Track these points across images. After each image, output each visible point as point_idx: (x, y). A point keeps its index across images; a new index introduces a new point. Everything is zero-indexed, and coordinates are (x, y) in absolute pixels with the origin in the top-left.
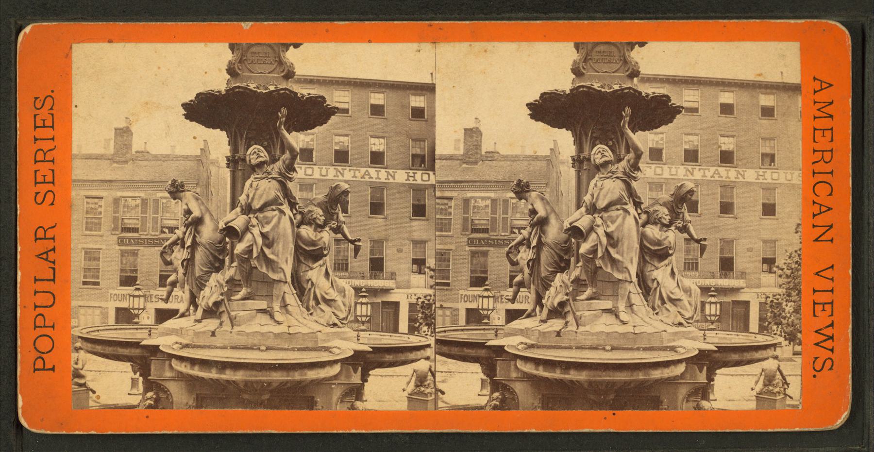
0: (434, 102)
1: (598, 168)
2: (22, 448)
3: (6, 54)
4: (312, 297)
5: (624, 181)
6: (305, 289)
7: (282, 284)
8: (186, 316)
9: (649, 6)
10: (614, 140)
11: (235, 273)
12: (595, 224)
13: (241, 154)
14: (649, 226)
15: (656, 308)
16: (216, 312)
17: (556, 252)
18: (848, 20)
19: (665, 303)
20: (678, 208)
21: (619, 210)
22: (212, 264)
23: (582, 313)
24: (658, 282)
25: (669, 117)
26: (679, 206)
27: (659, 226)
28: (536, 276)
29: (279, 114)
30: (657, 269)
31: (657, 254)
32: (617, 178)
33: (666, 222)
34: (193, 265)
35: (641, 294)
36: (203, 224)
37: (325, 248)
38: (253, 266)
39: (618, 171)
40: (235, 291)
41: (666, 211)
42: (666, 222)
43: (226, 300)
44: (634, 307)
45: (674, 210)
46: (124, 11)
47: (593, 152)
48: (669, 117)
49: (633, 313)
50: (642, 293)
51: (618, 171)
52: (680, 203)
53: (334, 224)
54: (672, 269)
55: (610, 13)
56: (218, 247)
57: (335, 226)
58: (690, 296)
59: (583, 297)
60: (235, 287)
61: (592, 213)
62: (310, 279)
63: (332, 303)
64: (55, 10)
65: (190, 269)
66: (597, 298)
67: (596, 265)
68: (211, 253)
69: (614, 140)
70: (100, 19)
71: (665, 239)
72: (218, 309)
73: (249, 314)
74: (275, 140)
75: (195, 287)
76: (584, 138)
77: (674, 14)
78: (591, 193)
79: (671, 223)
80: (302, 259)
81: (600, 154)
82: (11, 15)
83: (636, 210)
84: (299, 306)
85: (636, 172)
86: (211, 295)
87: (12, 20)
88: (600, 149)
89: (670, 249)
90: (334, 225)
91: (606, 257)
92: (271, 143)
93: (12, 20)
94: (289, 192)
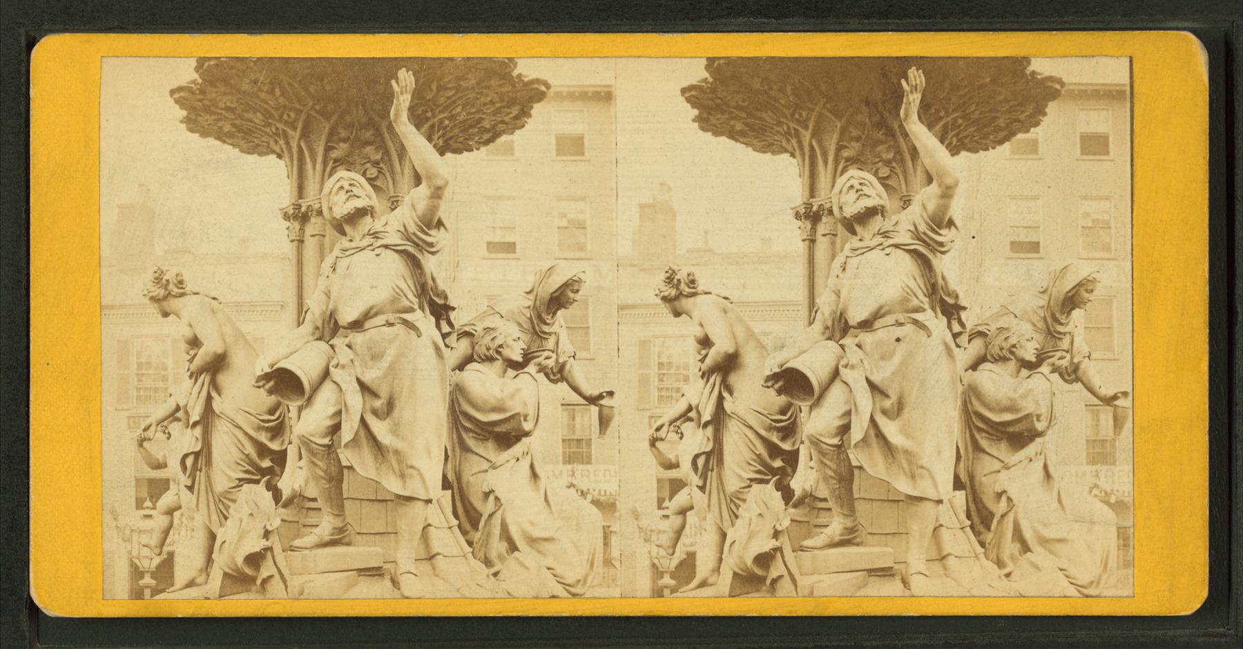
3: (13, 78)
4: (1009, 534)
5: (915, 253)
6: (992, 515)
7: (420, 504)
10: (381, 165)
11: (307, 482)
13: (310, 200)
14: (987, 366)
15: (496, 561)
16: (764, 579)
17: (246, 434)
18: (1206, 26)
19: (1029, 550)
21: (901, 324)
23: (816, 578)
24: (1009, 499)
25: (515, 111)
26: (548, 318)
28: (203, 492)
30: (494, 467)
31: (490, 432)
33: (1030, 356)
34: (209, 462)
35: (456, 530)
36: (228, 368)
37: (1038, 417)
41: (515, 331)
42: (1030, 356)
43: (278, 550)
44: (951, 561)
45: (533, 328)
47: (326, 190)
48: (1030, 109)
49: (948, 576)
50: (972, 527)
51: (388, 229)
52: (1063, 313)
54: (532, 467)
55: (868, 19)
56: (269, 421)
57: (1065, 363)
58: (578, 527)
59: (309, 539)
60: (306, 517)
63: (1059, 546)
65: (201, 477)
66: (346, 540)
67: (339, 461)
68: (251, 438)
69: (381, 165)
70: (146, 28)
71: (513, 396)
73: (347, 577)
74: (910, 164)
76: (309, 166)
77: (959, 19)
79: (528, 357)
84: (977, 557)
86: (241, 538)
87: (22, 31)
88: (852, 182)
89: (525, 420)
91: (364, 441)
92: (898, 170)
93: (22, 31)
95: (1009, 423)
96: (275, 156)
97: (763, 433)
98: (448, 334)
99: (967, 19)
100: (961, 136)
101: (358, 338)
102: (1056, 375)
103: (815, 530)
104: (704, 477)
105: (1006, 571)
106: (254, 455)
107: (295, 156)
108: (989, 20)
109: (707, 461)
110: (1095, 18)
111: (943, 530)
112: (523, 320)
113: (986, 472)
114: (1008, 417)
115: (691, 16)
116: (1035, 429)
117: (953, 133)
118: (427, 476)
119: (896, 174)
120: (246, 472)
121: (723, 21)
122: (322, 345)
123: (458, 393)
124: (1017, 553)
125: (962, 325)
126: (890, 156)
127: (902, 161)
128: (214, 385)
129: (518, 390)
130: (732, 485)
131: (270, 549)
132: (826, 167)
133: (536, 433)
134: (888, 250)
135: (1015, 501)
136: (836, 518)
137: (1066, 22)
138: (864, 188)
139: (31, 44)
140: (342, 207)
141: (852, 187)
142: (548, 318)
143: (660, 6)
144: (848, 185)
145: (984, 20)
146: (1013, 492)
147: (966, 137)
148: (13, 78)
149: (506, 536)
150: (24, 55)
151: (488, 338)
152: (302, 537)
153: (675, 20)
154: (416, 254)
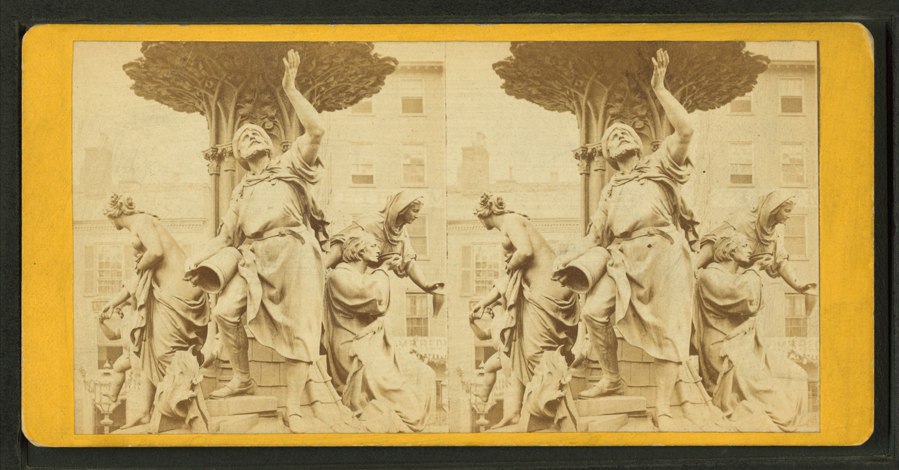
0: (291, 42)
1: (616, 162)
2: (27, 460)
3: (9, 57)
5: (661, 183)
6: (718, 373)
7: (304, 365)
8: (143, 424)
9: (668, 5)
11: (222, 349)
12: (610, 262)
13: (224, 145)
14: (714, 265)
15: (359, 406)
17: (178, 314)
18: (872, 19)
20: (768, 235)
21: (652, 235)
22: (182, 335)
23: (590, 418)
24: (730, 362)
26: (396, 231)
27: (361, 264)
28: (147, 357)
29: (653, 60)
30: (357, 338)
31: (355, 313)
32: (648, 178)
33: (745, 258)
34: (521, 334)
36: (165, 266)
37: (751, 302)
38: (249, 336)
39: (280, 165)
40: (590, 381)
41: (372, 240)
42: (745, 258)
43: (201, 398)
44: (688, 407)
45: (386, 237)
46: (130, 13)
47: (236, 138)
49: (685, 417)
50: (703, 382)
51: (280, 165)
53: (396, 259)
55: (628, 13)
56: (194, 305)
58: (418, 382)
60: (222, 374)
61: (606, 242)
62: (356, 356)
63: (766, 395)
64: (60, 12)
66: (250, 391)
67: (245, 334)
68: (181, 317)
70: (106, 21)
71: (371, 287)
72: (186, 411)
73: (251, 418)
75: (155, 374)
78: (234, 209)
80: (340, 320)
81: (248, 140)
82: (15, 17)
83: (317, 236)
84: (706, 403)
85: (313, 168)
88: (616, 132)
90: (768, 262)
91: (263, 319)
92: (650, 123)
93: (16, 22)
94: (311, 204)
95: (730, 307)
96: (199, 113)
97: (552, 313)
98: (324, 242)
99: (699, 14)
100: (695, 98)
101: (259, 245)
102: (764, 272)
103: (589, 384)
104: (509, 345)
105: (728, 413)
106: (184, 330)
107: (214, 113)
108: (715, 15)
109: (511, 334)
110: (792, 13)
111: (682, 384)
112: (378, 232)
113: (713, 341)
114: (729, 302)
115: (500, 11)
116: (749, 311)
117: (689, 96)
118: (309, 345)
119: (648, 126)
120: (549, 342)
121: (523, 15)
122: (233, 250)
123: (331, 285)
124: (735, 401)
125: (326, 235)
126: (644, 113)
127: (652, 117)
128: (155, 278)
129: (375, 283)
130: (530, 351)
131: (195, 398)
132: (597, 121)
133: (388, 314)
134: (642, 181)
135: (734, 363)
136: (605, 375)
137: (771, 16)
138: (256, 137)
139: (22, 32)
140: (248, 150)
141: (616, 135)
142: (396, 231)
143: (477, 4)
144: (613, 134)
145: (712, 14)
146: (732, 357)
147: (699, 99)
148: (9, 57)
149: (366, 388)
150: (17, 40)
151: (353, 244)
152: (219, 389)
153: (488, 14)
154: (301, 184)
